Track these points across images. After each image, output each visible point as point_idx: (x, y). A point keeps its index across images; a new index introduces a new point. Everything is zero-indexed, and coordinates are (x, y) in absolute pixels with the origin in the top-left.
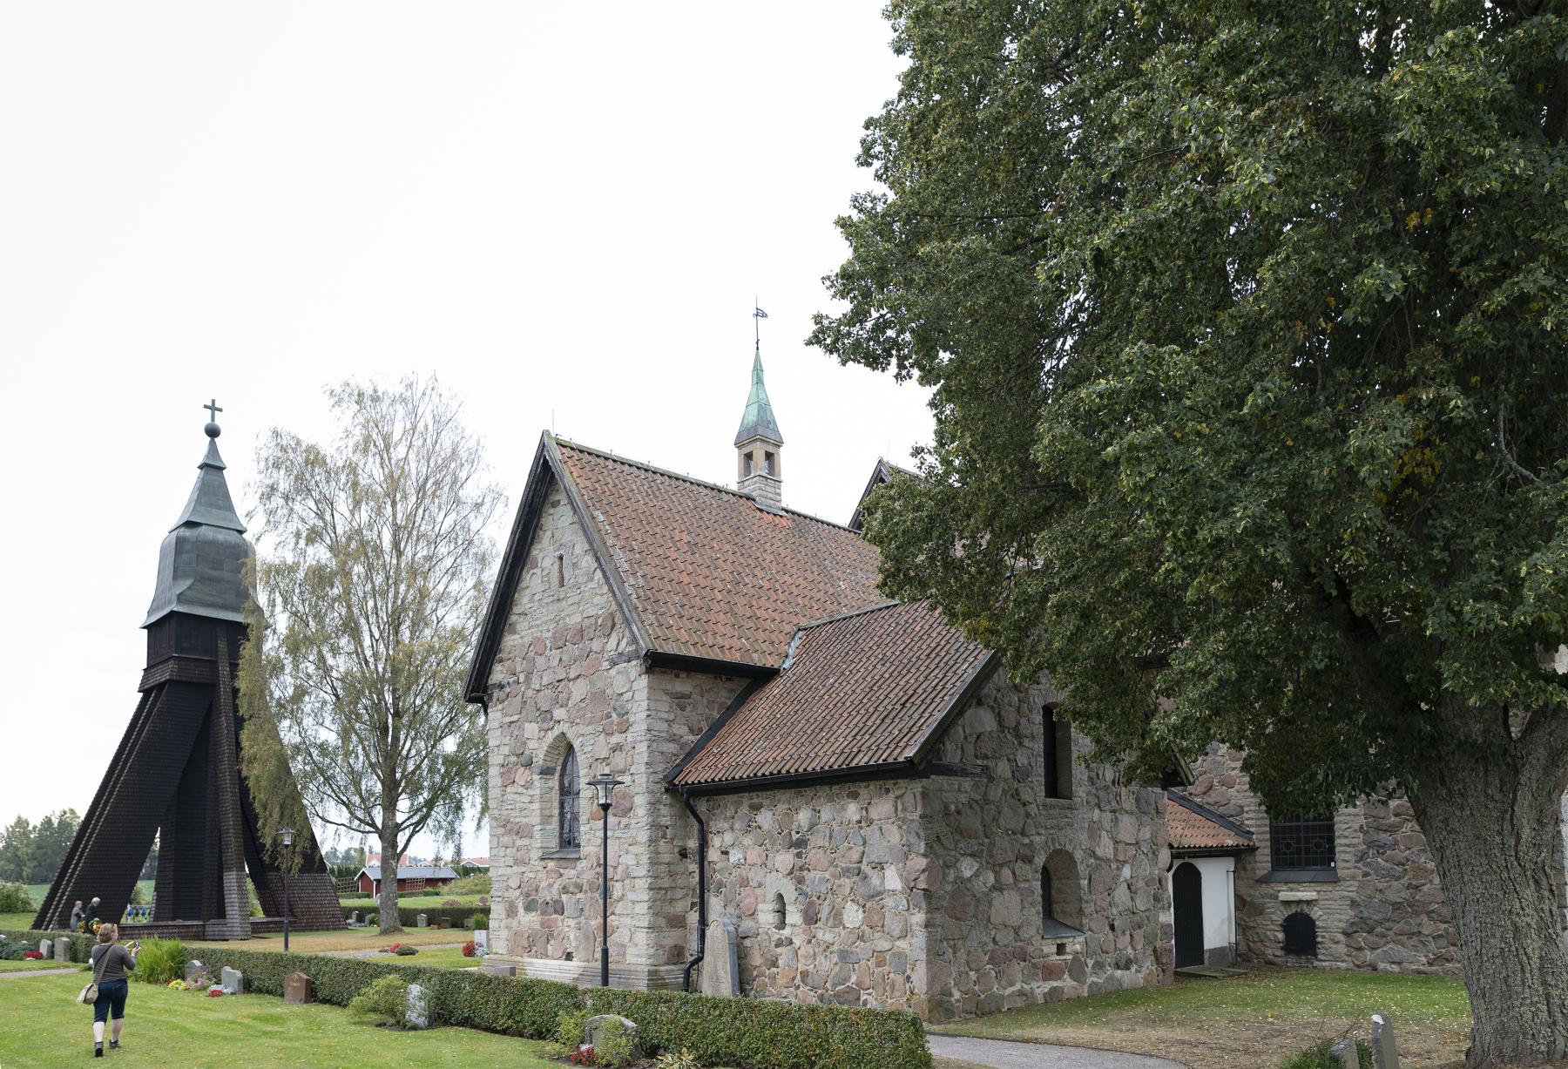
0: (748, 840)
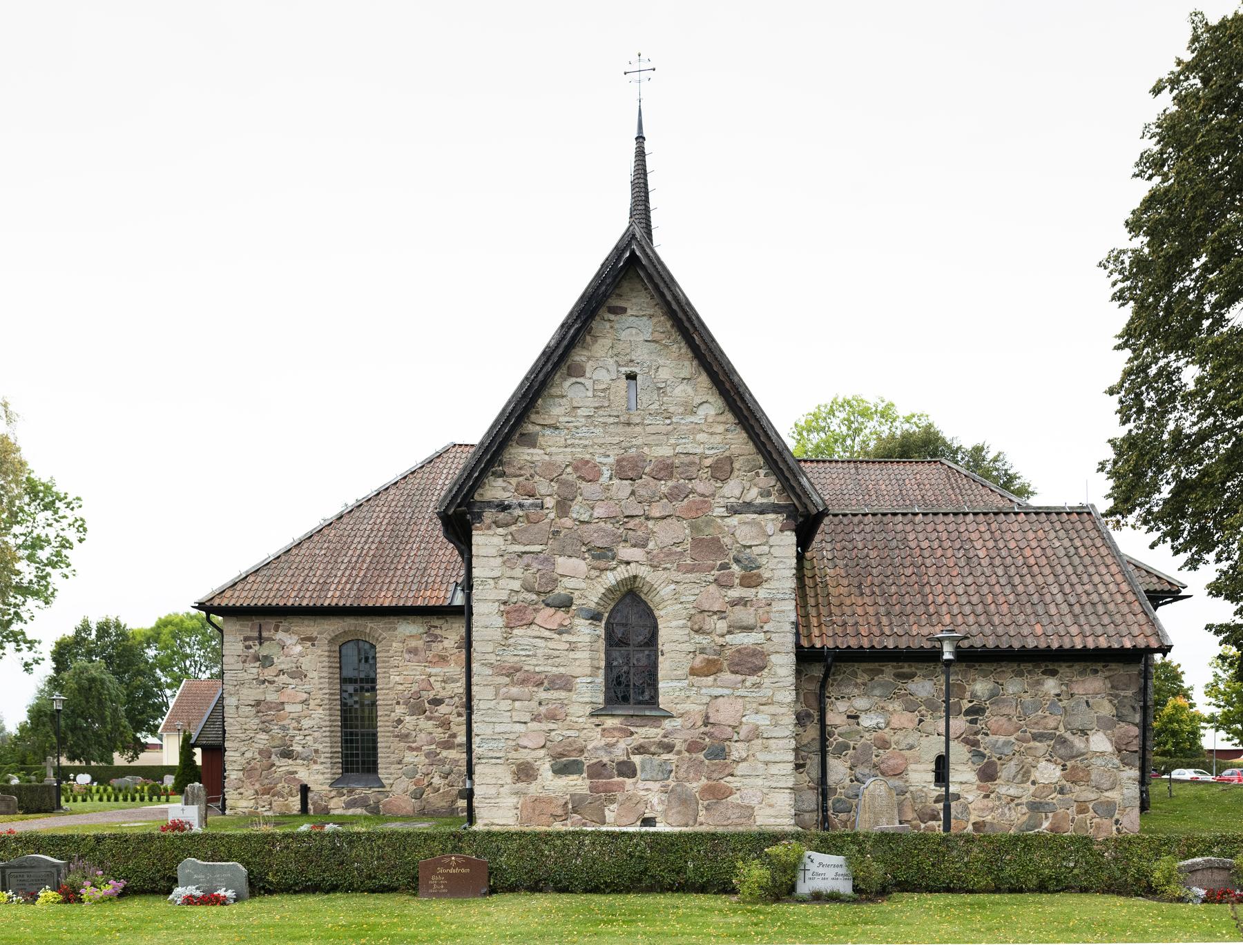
0: (896, 706)
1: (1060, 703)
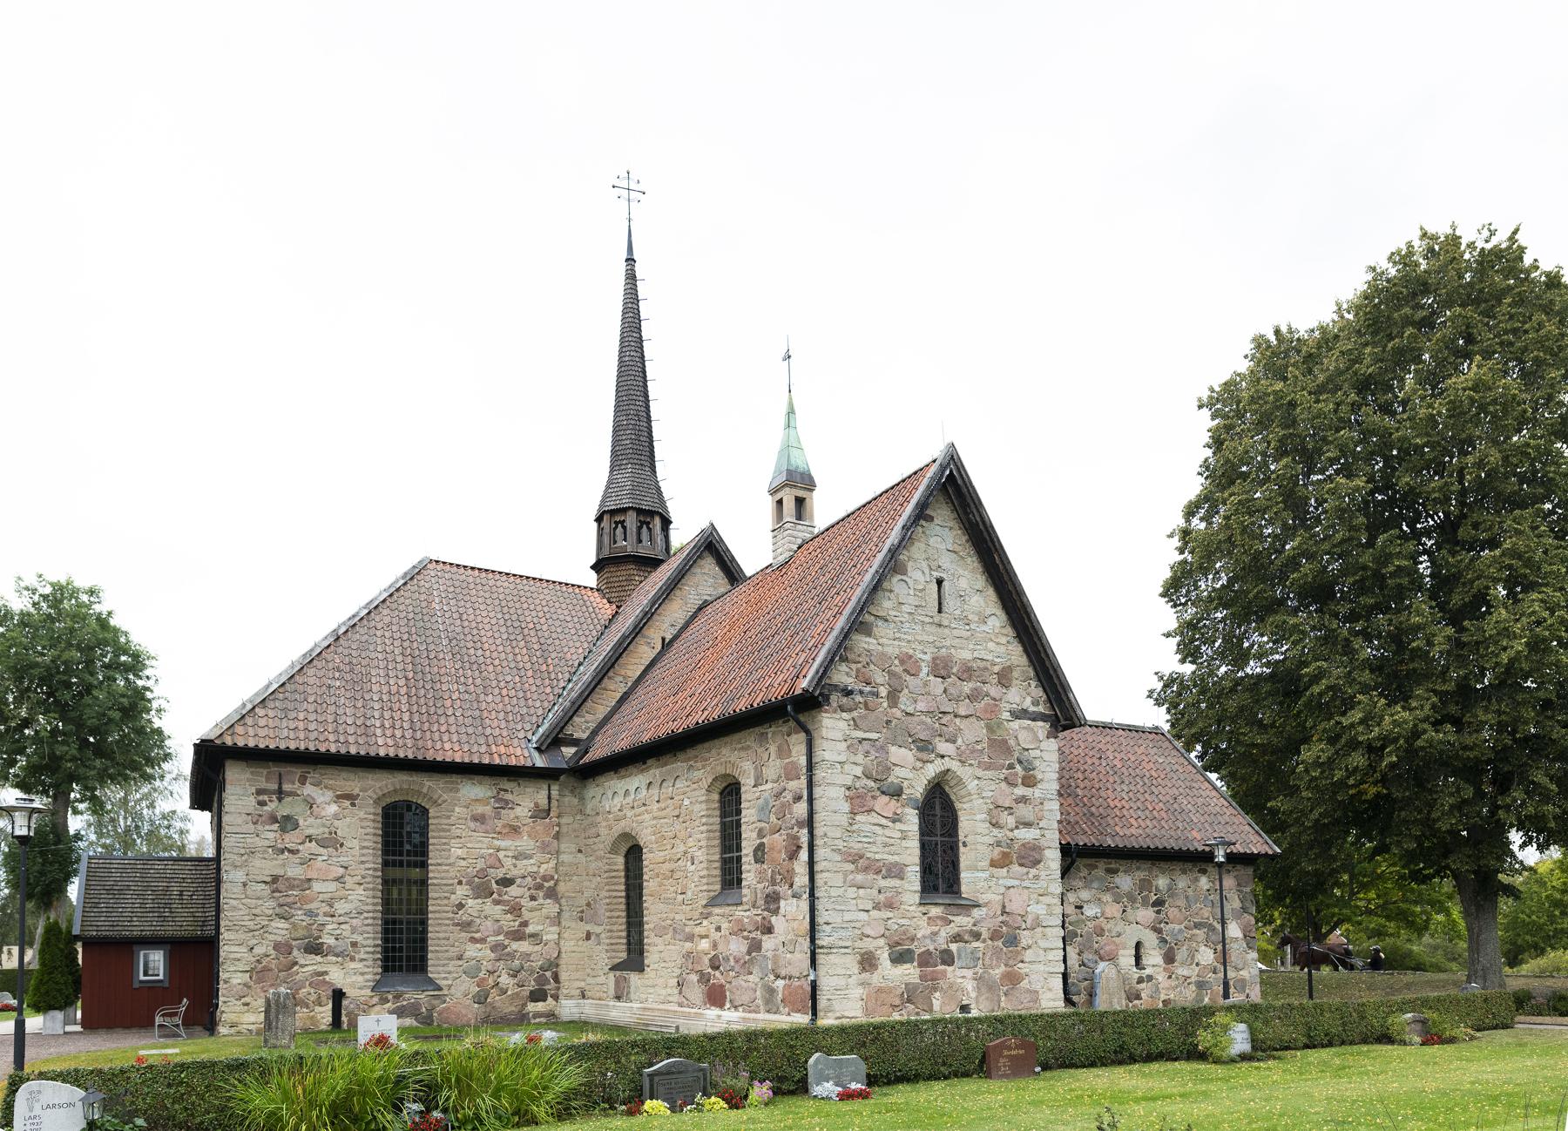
0: (1107, 897)
1: (689, 894)
